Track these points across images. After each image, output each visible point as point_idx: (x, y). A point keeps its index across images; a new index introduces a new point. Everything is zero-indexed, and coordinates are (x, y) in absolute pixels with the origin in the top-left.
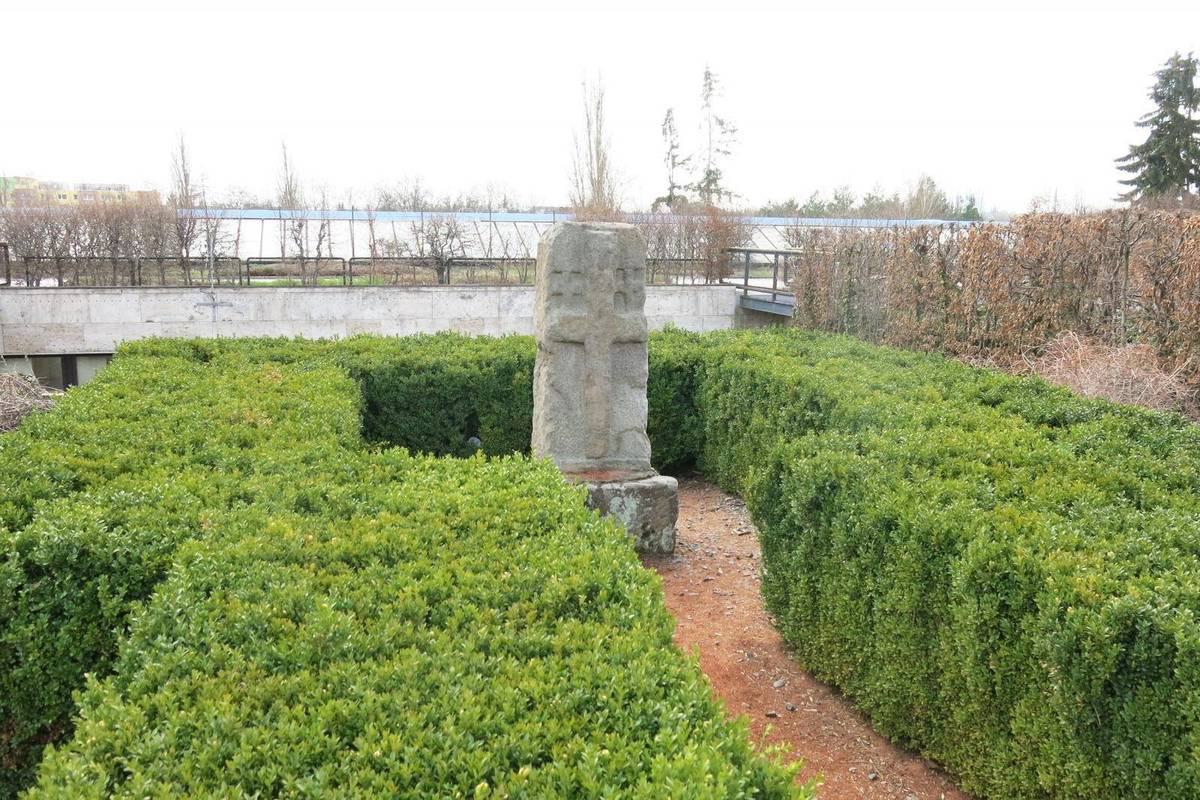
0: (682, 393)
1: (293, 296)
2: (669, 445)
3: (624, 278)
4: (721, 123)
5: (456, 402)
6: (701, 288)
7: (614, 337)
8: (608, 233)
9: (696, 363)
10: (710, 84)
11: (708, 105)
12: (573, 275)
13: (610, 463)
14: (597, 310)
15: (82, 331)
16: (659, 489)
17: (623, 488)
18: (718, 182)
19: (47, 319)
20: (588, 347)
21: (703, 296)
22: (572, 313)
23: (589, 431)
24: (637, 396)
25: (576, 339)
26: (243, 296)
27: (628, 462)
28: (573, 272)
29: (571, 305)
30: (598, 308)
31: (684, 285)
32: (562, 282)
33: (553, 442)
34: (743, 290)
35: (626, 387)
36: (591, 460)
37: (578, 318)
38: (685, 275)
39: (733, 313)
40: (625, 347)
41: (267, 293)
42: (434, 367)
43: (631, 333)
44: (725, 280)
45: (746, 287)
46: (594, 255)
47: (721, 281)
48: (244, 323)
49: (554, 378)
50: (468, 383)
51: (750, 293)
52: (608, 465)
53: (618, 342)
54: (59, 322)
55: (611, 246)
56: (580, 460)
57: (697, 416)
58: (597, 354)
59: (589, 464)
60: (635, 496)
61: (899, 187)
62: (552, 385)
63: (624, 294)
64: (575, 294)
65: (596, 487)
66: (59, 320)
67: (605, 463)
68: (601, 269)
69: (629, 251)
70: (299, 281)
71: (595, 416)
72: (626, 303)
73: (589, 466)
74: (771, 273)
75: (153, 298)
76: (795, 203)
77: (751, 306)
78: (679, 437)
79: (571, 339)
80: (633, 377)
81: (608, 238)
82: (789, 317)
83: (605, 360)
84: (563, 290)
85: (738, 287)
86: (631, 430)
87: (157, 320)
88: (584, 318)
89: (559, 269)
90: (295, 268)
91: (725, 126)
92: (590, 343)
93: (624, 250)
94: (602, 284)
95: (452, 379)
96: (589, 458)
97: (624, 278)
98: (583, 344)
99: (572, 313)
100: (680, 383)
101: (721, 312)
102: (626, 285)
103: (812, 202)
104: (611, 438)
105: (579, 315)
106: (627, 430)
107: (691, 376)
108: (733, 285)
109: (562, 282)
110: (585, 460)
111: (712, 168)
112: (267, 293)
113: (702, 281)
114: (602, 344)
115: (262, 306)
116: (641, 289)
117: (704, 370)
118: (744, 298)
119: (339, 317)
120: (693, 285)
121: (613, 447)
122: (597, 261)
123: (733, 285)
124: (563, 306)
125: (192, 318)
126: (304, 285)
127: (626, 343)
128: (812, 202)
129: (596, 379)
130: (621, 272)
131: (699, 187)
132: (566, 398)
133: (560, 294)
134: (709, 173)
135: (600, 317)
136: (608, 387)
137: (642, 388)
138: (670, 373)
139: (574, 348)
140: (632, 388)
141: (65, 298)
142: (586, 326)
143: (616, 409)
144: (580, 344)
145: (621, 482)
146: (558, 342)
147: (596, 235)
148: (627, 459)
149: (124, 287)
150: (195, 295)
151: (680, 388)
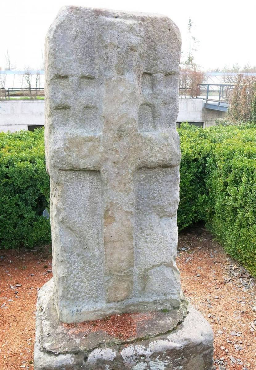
0: (197, 177)
1: (25, 104)
2: (186, 214)
3: (153, 85)
4: (194, 39)
5: (27, 189)
6: (189, 100)
7: (139, 161)
8: (130, 22)
9: (208, 156)
10: (191, 24)
11: (190, 32)
12: (85, 81)
13: (133, 305)
14: (116, 128)
17: (148, 353)
18: (193, 61)
20: (104, 176)
21: (190, 103)
22: (83, 133)
23: (109, 273)
24: (166, 227)
25: (90, 167)
26: (5, 104)
27: (155, 302)
28: (84, 77)
29: (83, 122)
30: (118, 125)
31: (182, 99)
32: (68, 91)
33: (66, 289)
34: (205, 101)
35: (154, 218)
36: (111, 305)
37: (91, 139)
38: (182, 95)
39: (201, 110)
40: (153, 173)
41: (15, 102)
42: (9, 162)
43: (160, 157)
44: (198, 97)
45: (207, 100)
46: (113, 53)
47: (197, 97)
48: (6, 115)
49: (63, 214)
50: (34, 175)
51: (209, 102)
52: (132, 308)
53: (144, 168)
55: (134, 40)
56: (99, 306)
57: (208, 194)
58: (116, 184)
60: (162, 358)
63: (152, 106)
64: (87, 107)
65: (114, 354)
67: (128, 306)
69: (160, 48)
70: (29, 97)
71: (116, 256)
72: (154, 117)
73: (110, 312)
74: (218, 94)
76: (219, 70)
77: (209, 107)
78: (194, 208)
79: (82, 167)
80: (162, 207)
81: (131, 29)
82: (226, 112)
83: (127, 192)
84: (69, 102)
85: (204, 99)
86: (159, 266)
88: (99, 140)
89: (62, 73)
90: (28, 92)
91: (195, 40)
92: (108, 169)
93: (152, 48)
94: (122, 94)
95: (20, 172)
96: (108, 302)
97: (153, 85)
98: (99, 171)
99: (83, 133)
100: (196, 170)
101: (197, 110)
102: (155, 95)
103: (225, 69)
104: (135, 278)
105: (92, 134)
107: (205, 167)
108: (202, 99)
109: (68, 91)
110: (104, 305)
111: (191, 56)
112: (15, 102)
113: (189, 97)
114: (123, 172)
116: (173, 99)
117: (215, 161)
118: (206, 104)
120: (185, 99)
121: (138, 286)
123: (202, 99)
124: (71, 123)
126: (31, 99)
127: (155, 168)
128: (225, 69)
129: (116, 215)
130: (147, 77)
131: (186, 63)
132: (80, 235)
133: (67, 107)
134: (190, 58)
135: (120, 137)
136: (133, 221)
137: (171, 216)
138: (188, 163)
139: (88, 178)
140: (161, 217)
142: (102, 149)
143: (141, 244)
144: (96, 172)
147: (114, 24)
148: (154, 298)
151: (195, 174)
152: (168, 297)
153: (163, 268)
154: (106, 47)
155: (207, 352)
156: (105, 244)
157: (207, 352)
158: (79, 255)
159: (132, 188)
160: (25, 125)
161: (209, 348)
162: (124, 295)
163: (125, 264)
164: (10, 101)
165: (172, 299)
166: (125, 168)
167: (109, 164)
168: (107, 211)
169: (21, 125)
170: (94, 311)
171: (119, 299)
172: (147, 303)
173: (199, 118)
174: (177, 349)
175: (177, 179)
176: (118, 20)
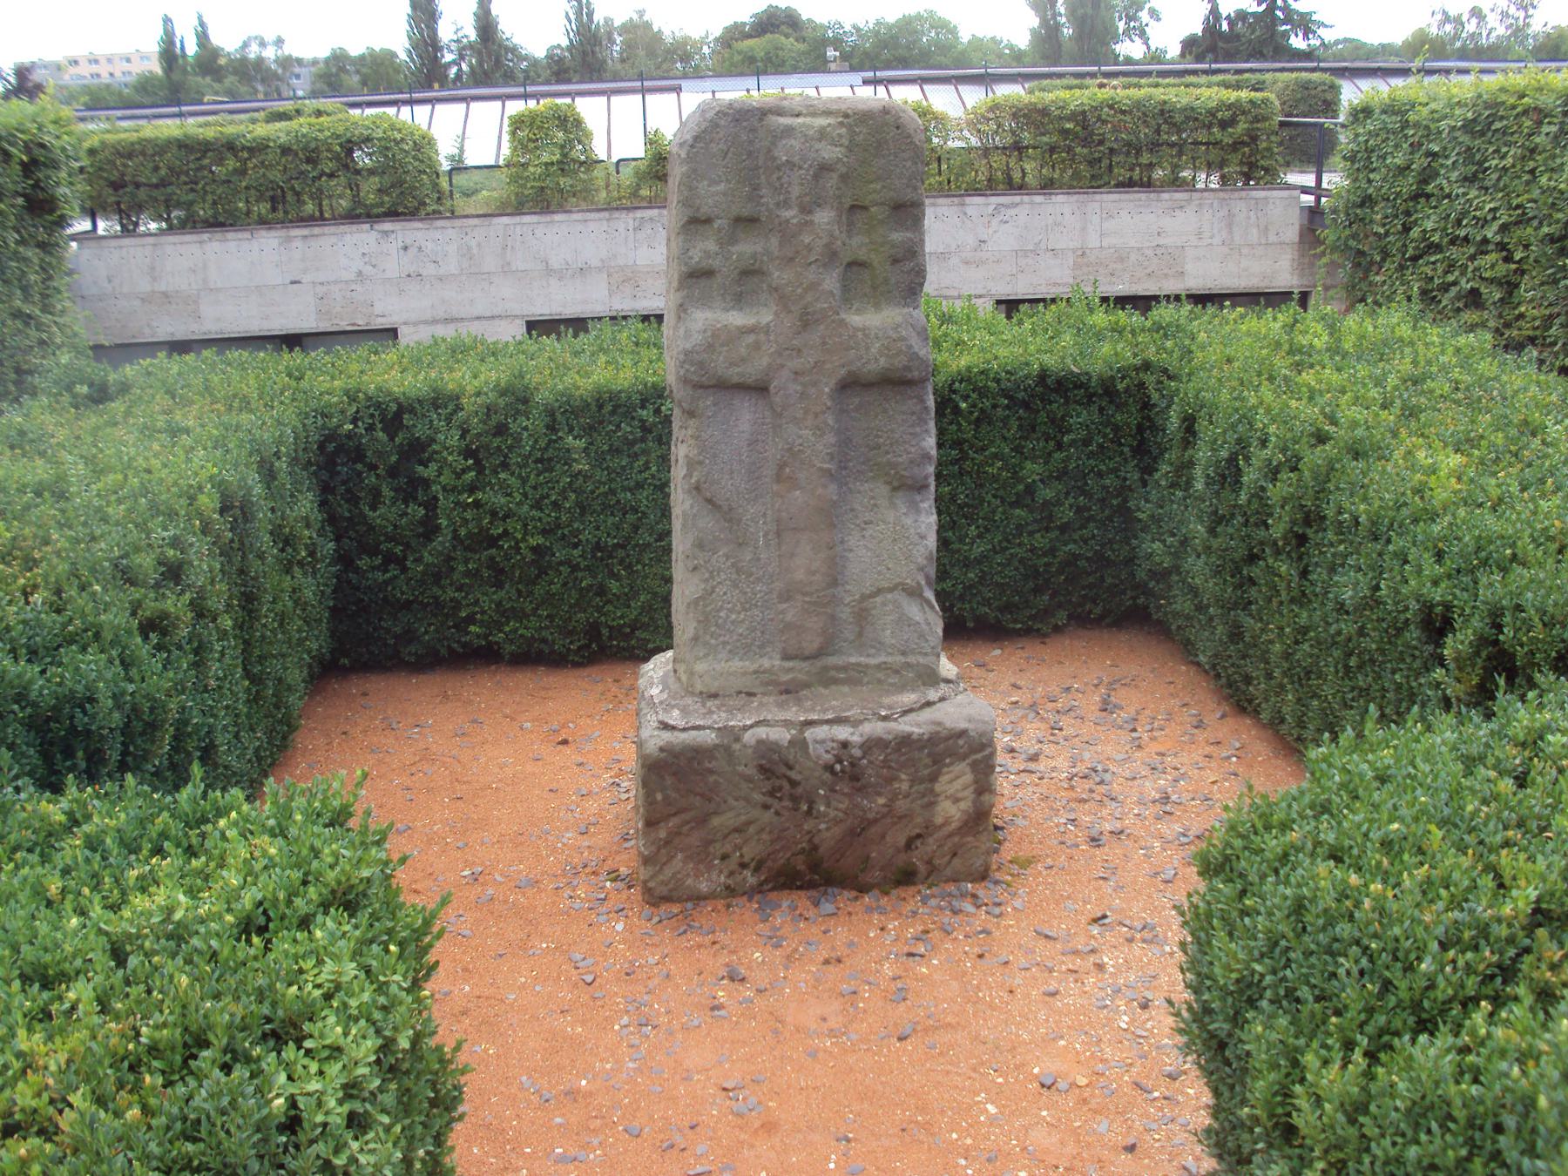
7: (843, 371)
8: (822, 121)
15: (196, 302)
16: (948, 739)
19: (144, 286)
22: (737, 319)
28: (738, 220)
29: (739, 300)
36: (790, 664)
37: (752, 330)
39: (1296, 239)
53: (851, 385)
54: (163, 288)
55: (829, 153)
58: (799, 414)
59: (790, 670)
61: (783, 6)
62: (697, 488)
66: (162, 287)
68: (806, 210)
73: (790, 676)
75: (298, 243)
79: (736, 380)
81: (822, 134)
85: (1305, 190)
86: (891, 590)
87: (306, 279)
88: (767, 330)
89: (702, 214)
94: (809, 248)
96: (786, 657)
101: (1272, 238)
106: (879, 591)
110: (777, 663)
115: (469, 248)
119: (595, 263)
122: (796, 191)
125: (360, 273)
141: (169, 249)
144: (760, 389)
145: (856, 723)
146: (702, 387)
149: (263, 222)
150: (364, 236)
152: (911, 659)
153: (898, 595)
154: (778, 168)
155: (979, 756)
156: (778, 534)
157: (979, 756)
158: (727, 557)
159: (830, 422)
160: (516, 316)
161: (983, 747)
162: (816, 645)
163: (818, 577)
164: (458, 223)
165: (918, 664)
166: (815, 384)
167: (785, 373)
168: (781, 467)
169: (500, 317)
170: (756, 672)
171: (807, 653)
172: (867, 666)
173: (1288, 276)
174: (915, 737)
175: (926, 408)
176: (800, 120)
